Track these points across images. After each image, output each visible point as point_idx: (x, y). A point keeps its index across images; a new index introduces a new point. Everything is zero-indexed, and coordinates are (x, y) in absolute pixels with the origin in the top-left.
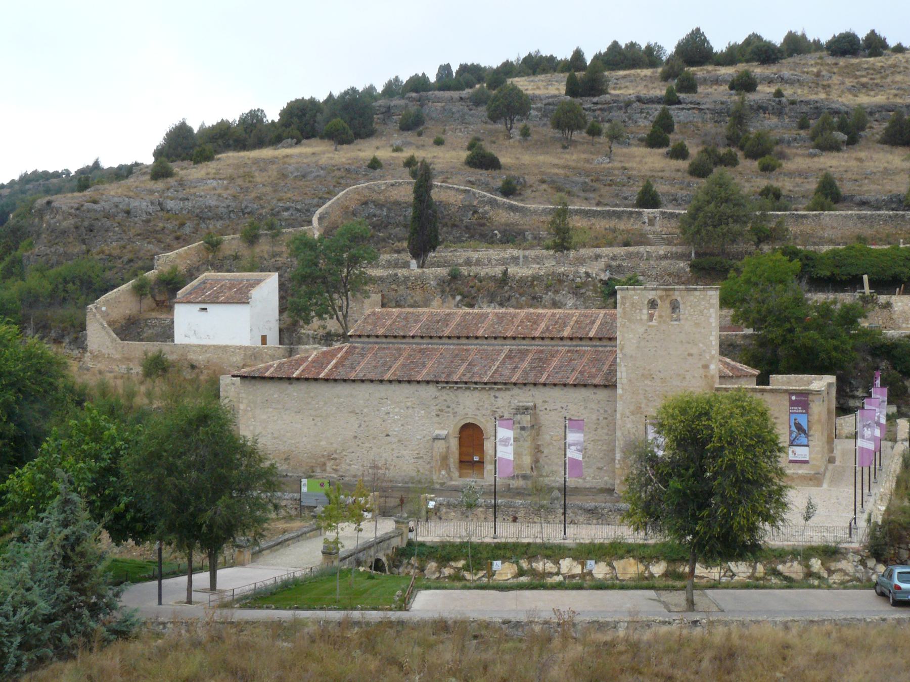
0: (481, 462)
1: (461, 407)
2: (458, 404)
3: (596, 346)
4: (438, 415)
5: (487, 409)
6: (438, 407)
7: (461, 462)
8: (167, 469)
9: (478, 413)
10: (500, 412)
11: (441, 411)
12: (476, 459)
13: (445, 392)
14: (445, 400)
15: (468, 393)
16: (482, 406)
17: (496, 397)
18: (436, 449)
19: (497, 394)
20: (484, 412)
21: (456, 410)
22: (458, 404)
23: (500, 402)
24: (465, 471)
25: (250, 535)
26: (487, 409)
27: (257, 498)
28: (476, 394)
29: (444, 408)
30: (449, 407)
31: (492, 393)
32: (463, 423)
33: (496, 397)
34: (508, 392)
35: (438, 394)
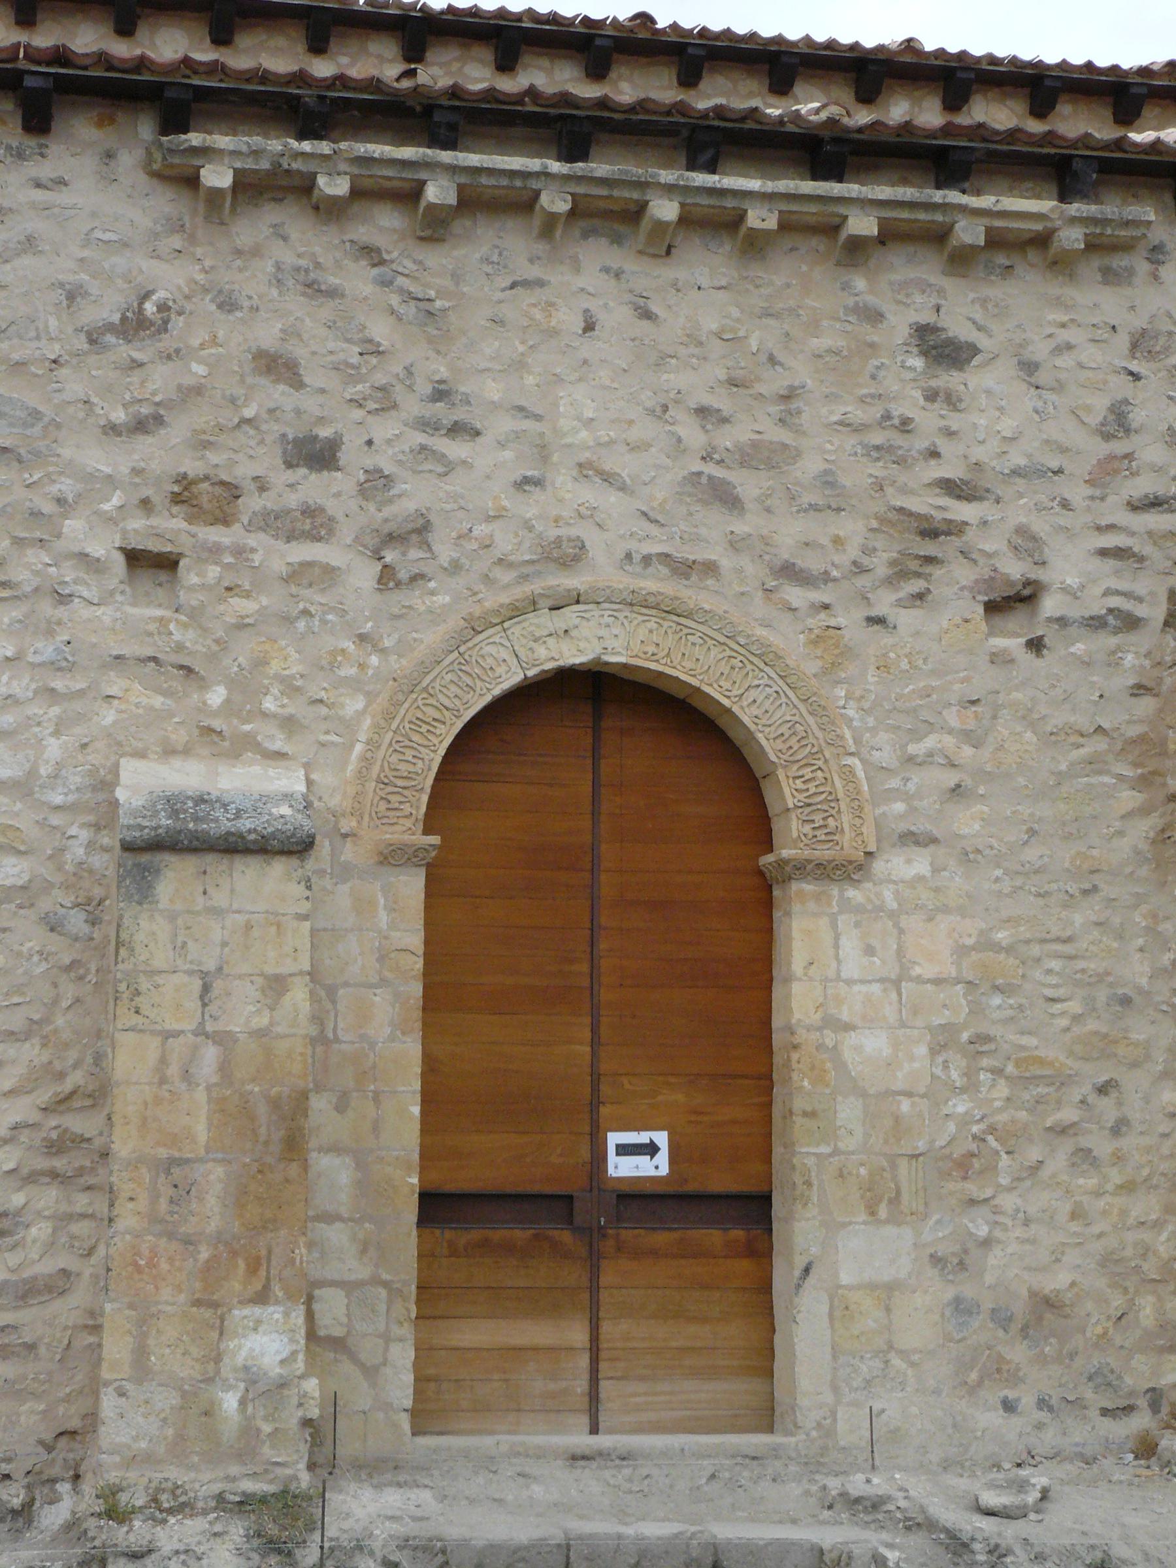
0: (730, 1214)
1: (489, 462)
2: (450, 419)
3: (370, 176)
4: (151, 564)
5: (831, 497)
6: (165, 454)
7: (435, 1206)
8: (174, 231)
9: (709, 536)
10: (991, 539)
11: (206, 498)
12: (638, 1158)
13: (284, 240)
14: (276, 366)
15: (592, 276)
16: (753, 456)
17: (942, 350)
18: (171, 1001)
19: (961, 308)
20: (789, 534)
21: (415, 494)
22: (450, 419)
23: (995, 415)
24: (474, 1333)
25: (215, 1122)
26: (831, 497)
27: (169, 818)
28: (702, 292)
29: (252, 461)
30: (318, 455)
31: (910, 292)
32: (505, 667)
33: (942, 350)
34: (1097, 302)
35: (169, 279)
